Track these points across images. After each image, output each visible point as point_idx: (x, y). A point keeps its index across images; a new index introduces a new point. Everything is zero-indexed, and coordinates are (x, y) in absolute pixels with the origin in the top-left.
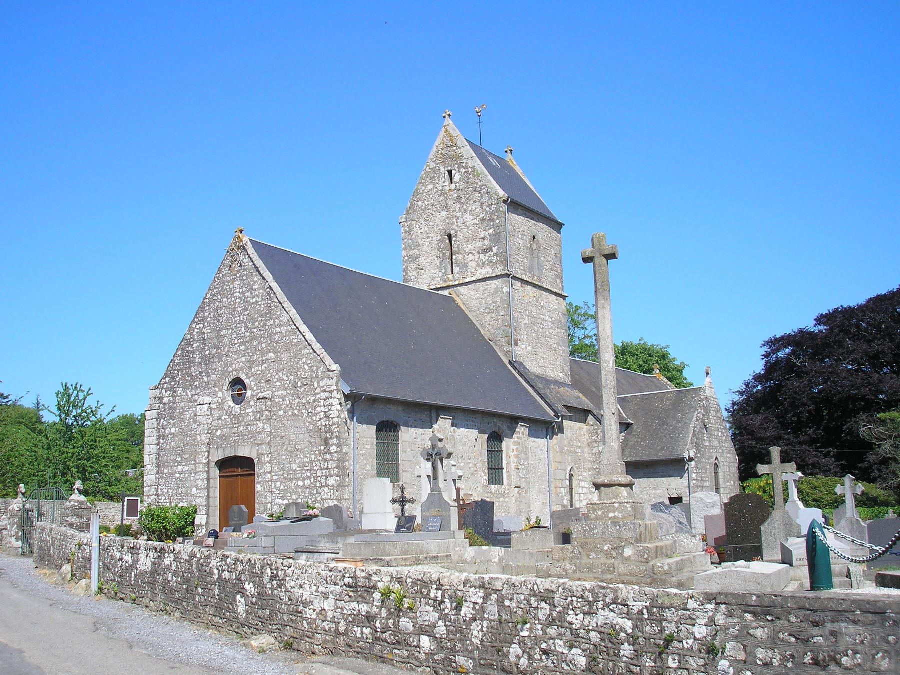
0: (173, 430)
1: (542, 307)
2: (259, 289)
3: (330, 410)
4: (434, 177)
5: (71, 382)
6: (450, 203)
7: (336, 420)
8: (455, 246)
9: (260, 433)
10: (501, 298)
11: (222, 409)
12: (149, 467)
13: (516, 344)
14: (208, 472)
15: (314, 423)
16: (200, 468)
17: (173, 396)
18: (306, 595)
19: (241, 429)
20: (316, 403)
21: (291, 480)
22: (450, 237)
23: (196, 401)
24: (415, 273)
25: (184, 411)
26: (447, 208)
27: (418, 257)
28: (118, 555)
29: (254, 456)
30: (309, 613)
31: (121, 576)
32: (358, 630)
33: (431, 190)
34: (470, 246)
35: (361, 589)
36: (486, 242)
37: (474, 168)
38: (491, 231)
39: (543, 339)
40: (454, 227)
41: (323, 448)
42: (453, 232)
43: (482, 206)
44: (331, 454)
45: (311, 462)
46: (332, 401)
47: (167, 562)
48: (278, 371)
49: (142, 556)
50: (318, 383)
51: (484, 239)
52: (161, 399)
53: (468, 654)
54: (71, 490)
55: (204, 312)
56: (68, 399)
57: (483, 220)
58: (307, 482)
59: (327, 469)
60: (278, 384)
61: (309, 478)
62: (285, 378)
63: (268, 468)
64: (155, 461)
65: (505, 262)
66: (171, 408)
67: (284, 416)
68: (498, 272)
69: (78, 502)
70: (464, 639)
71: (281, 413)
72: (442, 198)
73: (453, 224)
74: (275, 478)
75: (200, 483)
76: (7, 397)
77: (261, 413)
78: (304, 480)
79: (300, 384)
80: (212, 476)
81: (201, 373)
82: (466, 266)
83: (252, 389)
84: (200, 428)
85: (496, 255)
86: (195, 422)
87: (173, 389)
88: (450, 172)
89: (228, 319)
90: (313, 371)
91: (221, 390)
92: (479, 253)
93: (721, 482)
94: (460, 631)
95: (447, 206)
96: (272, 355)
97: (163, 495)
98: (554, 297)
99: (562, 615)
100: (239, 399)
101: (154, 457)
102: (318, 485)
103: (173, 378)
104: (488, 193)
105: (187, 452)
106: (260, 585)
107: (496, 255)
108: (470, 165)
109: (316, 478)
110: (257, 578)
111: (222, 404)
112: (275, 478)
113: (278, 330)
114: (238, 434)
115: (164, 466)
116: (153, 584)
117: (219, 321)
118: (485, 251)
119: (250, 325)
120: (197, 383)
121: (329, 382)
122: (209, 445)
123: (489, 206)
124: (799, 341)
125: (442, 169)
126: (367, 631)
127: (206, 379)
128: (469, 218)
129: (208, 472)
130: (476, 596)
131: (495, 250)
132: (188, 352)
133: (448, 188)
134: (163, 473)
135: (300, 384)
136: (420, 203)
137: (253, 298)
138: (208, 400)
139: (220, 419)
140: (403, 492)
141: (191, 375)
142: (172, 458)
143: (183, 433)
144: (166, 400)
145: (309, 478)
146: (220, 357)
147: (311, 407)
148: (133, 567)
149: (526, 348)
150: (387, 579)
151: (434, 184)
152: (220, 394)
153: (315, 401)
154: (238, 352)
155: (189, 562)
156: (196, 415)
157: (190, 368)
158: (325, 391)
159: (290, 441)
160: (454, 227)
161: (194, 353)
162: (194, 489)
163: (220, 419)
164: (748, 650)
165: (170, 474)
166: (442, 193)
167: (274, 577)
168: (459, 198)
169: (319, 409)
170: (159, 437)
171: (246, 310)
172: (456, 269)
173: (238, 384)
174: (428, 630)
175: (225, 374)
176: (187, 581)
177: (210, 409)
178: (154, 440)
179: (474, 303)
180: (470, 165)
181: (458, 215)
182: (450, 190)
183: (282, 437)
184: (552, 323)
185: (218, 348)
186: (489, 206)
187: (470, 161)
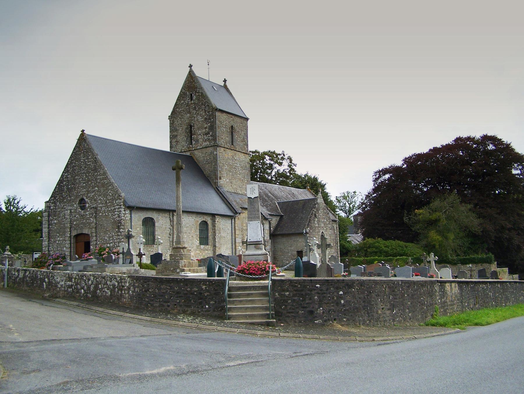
0: (55, 221)
2: (91, 158)
6: (191, 110)
9: (92, 223)
11: (76, 212)
12: (45, 238)
13: (220, 179)
15: (114, 219)
16: (67, 238)
17: (55, 206)
18: (58, 280)
21: (105, 244)
26: (189, 112)
27: (177, 136)
28: (14, 273)
29: (89, 233)
30: (59, 286)
33: (183, 103)
35: (70, 278)
39: (235, 175)
43: (205, 111)
45: (113, 236)
47: (27, 274)
48: (99, 196)
51: (206, 128)
53: (90, 293)
57: (206, 119)
58: (111, 245)
61: (112, 243)
66: (54, 211)
70: (89, 290)
75: (67, 245)
77: (92, 214)
82: (197, 141)
85: (211, 136)
86: (65, 218)
88: (191, 95)
89: (78, 172)
91: (75, 204)
94: (89, 288)
96: (96, 188)
97: (51, 251)
98: (243, 154)
99: (106, 282)
100: (83, 208)
104: (208, 106)
105: (62, 231)
106: (49, 279)
107: (211, 136)
109: (114, 243)
110: (48, 277)
111: (76, 210)
116: (23, 281)
118: (207, 134)
121: (120, 201)
123: (209, 112)
124: (394, 170)
125: (188, 93)
130: (92, 278)
131: (211, 133)
133: (190, 103)
137: (89, 162)
139: (75, 216)
143: (60, 223)
146: (75, 188)
148: (18, 276)
152: (75, 206)
154: (83, 187)
155: (33, 273)
158: (118, 205)
163: (75, 216)
166: (188, 105)
167: (52, 276)
168: (195, 108)
171: (85, 168)
175: (77, 196)
177: (71, 212)
181: (195, 116)
182: (191, 104)
184: (241, 167)
185: (74, 184)
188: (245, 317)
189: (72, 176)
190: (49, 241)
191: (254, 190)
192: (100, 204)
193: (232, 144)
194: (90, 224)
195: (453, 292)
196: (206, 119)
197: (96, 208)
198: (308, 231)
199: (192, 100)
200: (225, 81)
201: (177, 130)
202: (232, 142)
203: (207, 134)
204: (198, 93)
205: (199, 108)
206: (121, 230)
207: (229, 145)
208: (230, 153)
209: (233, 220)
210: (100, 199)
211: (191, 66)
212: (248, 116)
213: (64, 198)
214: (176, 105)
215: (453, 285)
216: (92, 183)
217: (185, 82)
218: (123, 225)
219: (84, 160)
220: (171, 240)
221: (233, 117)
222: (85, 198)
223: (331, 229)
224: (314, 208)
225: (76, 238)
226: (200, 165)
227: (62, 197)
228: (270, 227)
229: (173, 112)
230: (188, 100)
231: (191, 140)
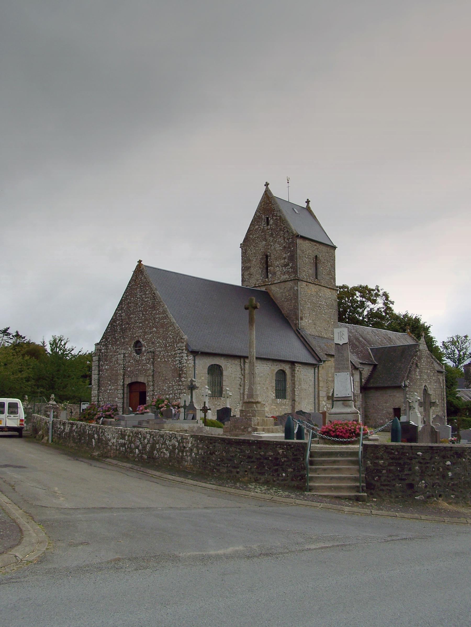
2: (149, 294)
3: (182, 359)
4: (259, 221)
5: (58, 335)
6: (267, 237)
7: (185, 364)
8: (270, 262)
9: (148, 370)
10: (293, 293)
16: (120, 387)
17: (106, 349)
19: (140, 367)
20: (175, 356)
21: (163, 395)
23: (118, 352)
24: (248, 277)
25: (112, 357)
27: (250, 267)
28: (59, 426)
29: (146, 382)
30: (110, 444)
31: (60, 435)
32: (122, 448)
34: (277, 262)
35: (123, 435)
36: (286, 260)
38: (289, 254)
40: (269, 251)
41: (178, 379)
42: (268, 254)
43: (284, 238)
44: (182, 382)
45: (173, 386)
46: (183, 354)
47: (74, 428)
48: (158, 338)
49: (67, 426)
50: (177, 345)
51: (285, 258)
52: (100, 350)
53: (145, 454)
54: (49, 400)
55: (122, 305)
57: (285, 247)
59: (180, 389)
60: (158, 344)
61: (172, 394)
62: (161, 341)
63: (151, 388)
64: (97, 383)
65: (295, 272)
66: (105, 355)
67: (160, 361)
69: (52, 404)
71: (159, 360)
72: (263, 234)
73: (268, 249)
74: (156, 393)
75: (119, 395)
76: (24, 337)
78: (169, 395)
79: (168, 345)
81: (120, 337)
82: (274, 274)
83: (145, 347)
84: (120, 367)
85: (291, 268)
86: (117, 363)
87: (106, 345)
88: (268, 218)
89: (133, 309)
90: (174, 339)
92: (282, 266)
94: (144, 447)
95: (265, 239)
96: (154, 329)
97: (101, 401)
98: (329, 290)
100: (139, 352)
101: (97, 381)
102: (176, 397)
103: (107, 340)
106: (98, 435)
107: (291, 268)
110: (97, 433)
111: (130, 354)
112: (156, 393)
113: (158, 316)
114: (138, 370)
116: (69, 437)
117: (129, 310)
118: (286, 265)
120: (118, 343)
121: (182, 345)
123: (288, 239)
125: (263, 217)
126: (124, 448)
127: (122, 340)
128: (277, 246)
130: (148, 436)
131: (291, 265)
132: (114, 325)
133: (266, 228)
134: (101, 390)
135: (168, 345)
136: (251, 236)
137: (146, 298)
138: (123, 351)
140: (185, 403)
141: (115, 338)
142: (107, 382)
144: (103, 351)
145: (172, 394)
146: (130, 329)
147: (173, 357)
148: (64, 431)
150: (129, 432)
151: (259, 225)
152: (130, 349)
153: (175, 354)
154: (139, 327)
156: (117, 359)
157: (115, 334)
158: (179, 349)
159: (163, 374)
160: (269, 251)
161: (117, 326)
162: (117, 399)
165: (105, 390)
167: (102, 432)
169: (177, 358)
170: (99, 371)
171: (142, 304)
172: (270, 275)
173: (138, 344)
174: (137, 447)
175: (132, 338)
176: (79, 435)
177: (124, 356)
178: (96, 372)
179: (279, 295)
180: (278, 215)
181: (272, 243)
182: (268, 229)
183: (159, 372)
185: (128, 324)
187: (278, 213)
189: (126, 315)
191: (343, 335)
193: (316, 278)
194: (146, 370)
197: (154, 352)
198: (407, 383)
199: (268, 225)
200: (308, 202)
201: (250, 261)
203: (286, 265)
204: (276, 216)
205: (277, 235)
207: (312, 279)
211: (267, 185)
212: (335, 244)
213: (117, 340)
217: (260, 203)
221: (318, 245)
222: (141, 340)
224: (415, 356)
226: (277, 302)
228: (361, 379)
230: (263, 224)
231: (267, 272)
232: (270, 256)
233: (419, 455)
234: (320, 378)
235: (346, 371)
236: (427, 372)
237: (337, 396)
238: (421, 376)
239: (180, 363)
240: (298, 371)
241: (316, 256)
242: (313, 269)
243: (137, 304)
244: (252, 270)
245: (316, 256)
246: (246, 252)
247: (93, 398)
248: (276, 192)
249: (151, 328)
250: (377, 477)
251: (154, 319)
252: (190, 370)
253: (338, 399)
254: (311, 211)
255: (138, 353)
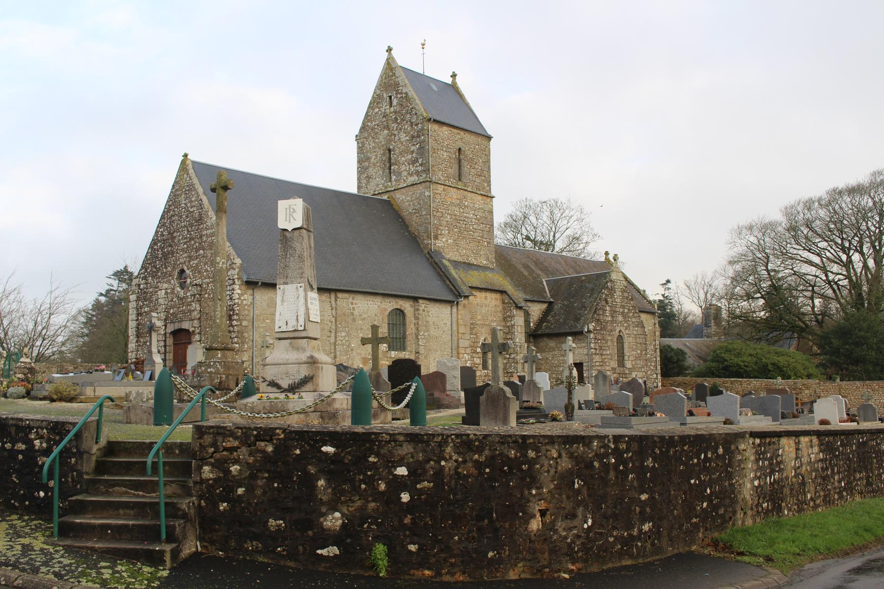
0: (146, 309)
1: (467, 206)
6: (390, 122)
14: (165, 341)
17: (146, 284)
22: (390, 150)
26: (387, 127)
27: (367, 168)
36: (414, 155)
37: (406, 93)
48: (206, 264)
51: (413, 152)
52: (139, 285)
56: (644, 291)
65: (427, 171)
68: (422, 179)
71: (206, 296)
80: (168, 343)
82: (399, 174)
85: (421, 165)
88: (390, 97)
93: (626, 350)
96: (201, 251)
98: (480, 198)
101: (134, 330)
103: (146, 270)
107: (421, 165)
108: (404, 91)
111: (173, 289)
114: (183, 312)
115: (142, 337)
119: (190, 229)
122: (165, 320)
129: (165, 341)
131: (420, 160)
141: (155, 267)
144: (142, 286)
149: (447, 241)
154: (183, 250)
164: (139, 421)
168: (396, 119)
171: (187, 217)
172: (394, 178)
177: (166, 293)
181: (396, 132)
185: (171, 246)
186: (416, 125)
188: (120, 531)
189: (169, 233)
190: (137, 342)
191: (294, 211)
192: (205, 278)
193: (460, 180)
194: (191, 311)
195: (805, 460)
196: (413, 137)
197: (200, 286)
198: (591, 328)
199: (391, 106)
200: (454, 76)
201: (368, 159)
202: (460, 175)
203: (414, 162)
204: (401, 93)
205: (403, 120)
206: (235, 323)
207: (452, 181)
208: (454, 194)
209: (454, 310)
210: (207, 271)
211: (389, 50)
212: (490, 132)
213: (158, 270)
214: (367, 115)
215: (804, 440)
216: (195, 242)
217: (381, 77)
218: (237, 314)
219: (186, 204)
220: (332, 340)
221: (462, 133)
222: (185, 268)
223: (637, 326)
224: (605, 288)
225: (174, 337)
226: (404, 214)
227: (155, 267)
228: (527, 322)
229: (363, 128)
230: (385, 107)
231: (390, 173)
232: (394, 150)
233: (326, 453)
234: (461, 322)
235: (299, 280)
236: (623, 312)
237: (280, 330)
238: (613, 317)
239: (231, 299)
240: (424, 311)
241: (460, 149)
242: (456, 166)
243: (181, 217)
244: (371, 171)
245: (460, 149)
246: (363, 146)
247: (130, 354)
248: (405, 59)
249: (197, 250)
250: (225, 504)
251: (201, 237)
252: (245, 310)
253: (283, 335)
254: (458, 88)
255: (182, 288)
